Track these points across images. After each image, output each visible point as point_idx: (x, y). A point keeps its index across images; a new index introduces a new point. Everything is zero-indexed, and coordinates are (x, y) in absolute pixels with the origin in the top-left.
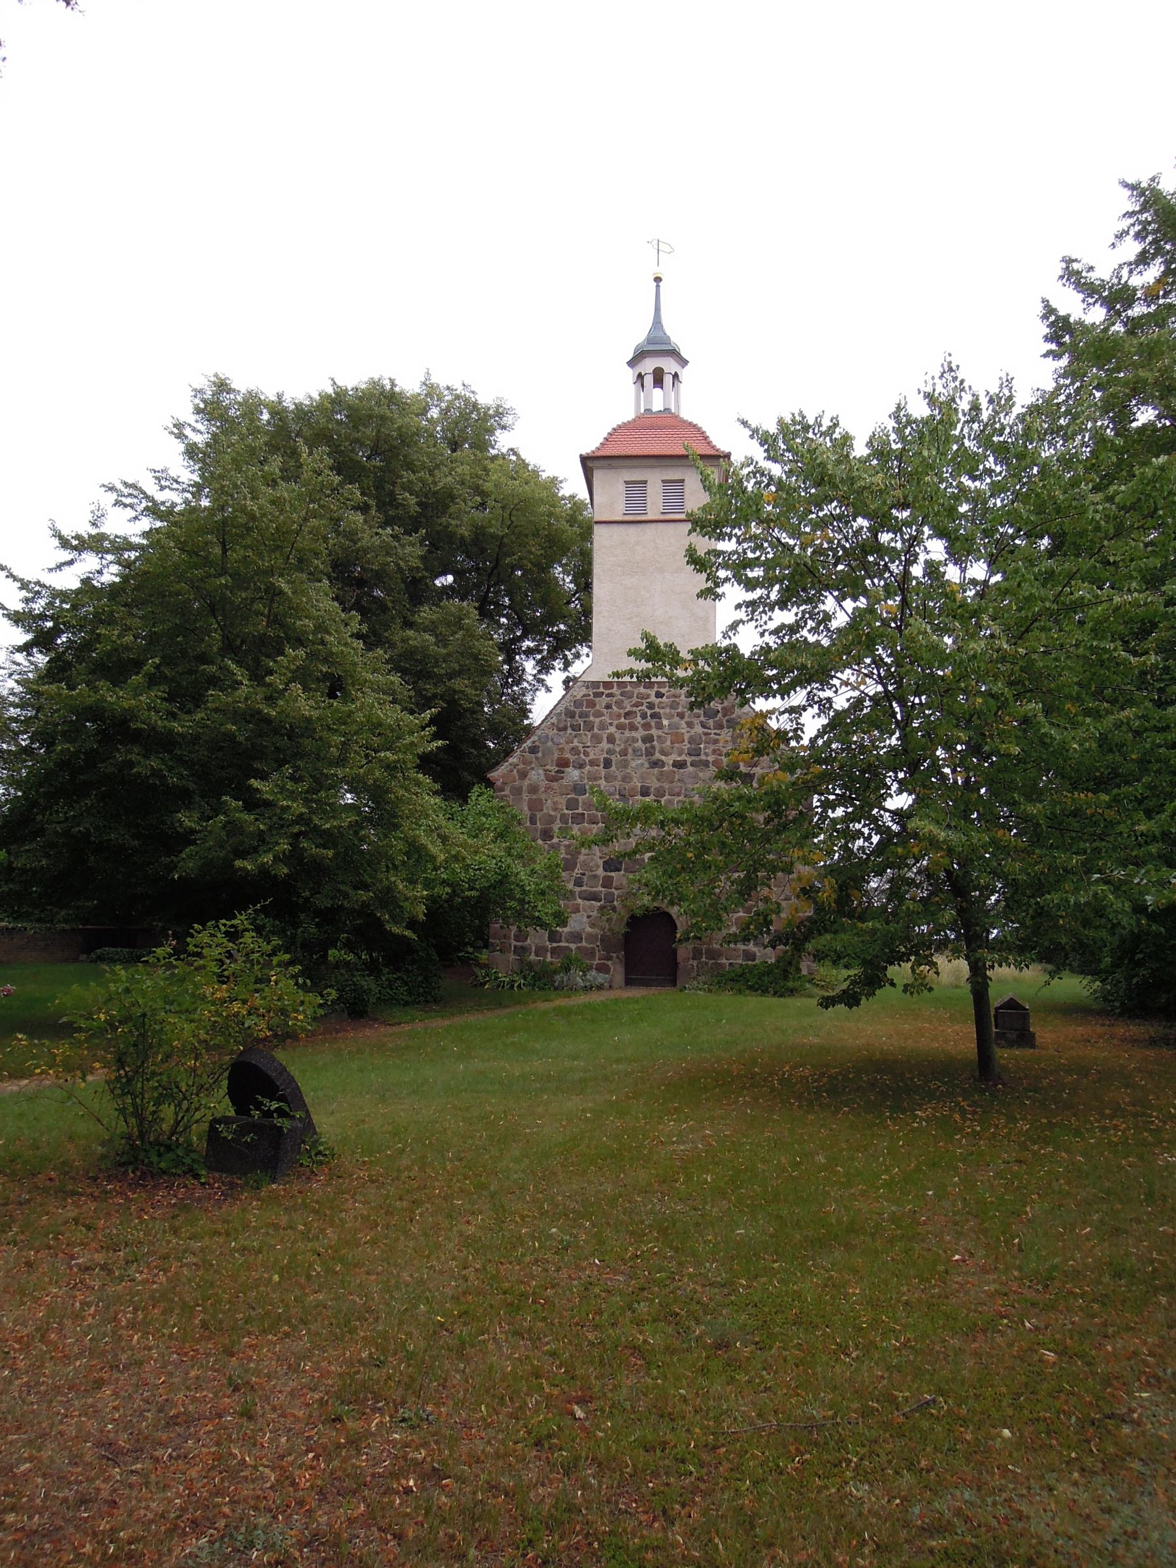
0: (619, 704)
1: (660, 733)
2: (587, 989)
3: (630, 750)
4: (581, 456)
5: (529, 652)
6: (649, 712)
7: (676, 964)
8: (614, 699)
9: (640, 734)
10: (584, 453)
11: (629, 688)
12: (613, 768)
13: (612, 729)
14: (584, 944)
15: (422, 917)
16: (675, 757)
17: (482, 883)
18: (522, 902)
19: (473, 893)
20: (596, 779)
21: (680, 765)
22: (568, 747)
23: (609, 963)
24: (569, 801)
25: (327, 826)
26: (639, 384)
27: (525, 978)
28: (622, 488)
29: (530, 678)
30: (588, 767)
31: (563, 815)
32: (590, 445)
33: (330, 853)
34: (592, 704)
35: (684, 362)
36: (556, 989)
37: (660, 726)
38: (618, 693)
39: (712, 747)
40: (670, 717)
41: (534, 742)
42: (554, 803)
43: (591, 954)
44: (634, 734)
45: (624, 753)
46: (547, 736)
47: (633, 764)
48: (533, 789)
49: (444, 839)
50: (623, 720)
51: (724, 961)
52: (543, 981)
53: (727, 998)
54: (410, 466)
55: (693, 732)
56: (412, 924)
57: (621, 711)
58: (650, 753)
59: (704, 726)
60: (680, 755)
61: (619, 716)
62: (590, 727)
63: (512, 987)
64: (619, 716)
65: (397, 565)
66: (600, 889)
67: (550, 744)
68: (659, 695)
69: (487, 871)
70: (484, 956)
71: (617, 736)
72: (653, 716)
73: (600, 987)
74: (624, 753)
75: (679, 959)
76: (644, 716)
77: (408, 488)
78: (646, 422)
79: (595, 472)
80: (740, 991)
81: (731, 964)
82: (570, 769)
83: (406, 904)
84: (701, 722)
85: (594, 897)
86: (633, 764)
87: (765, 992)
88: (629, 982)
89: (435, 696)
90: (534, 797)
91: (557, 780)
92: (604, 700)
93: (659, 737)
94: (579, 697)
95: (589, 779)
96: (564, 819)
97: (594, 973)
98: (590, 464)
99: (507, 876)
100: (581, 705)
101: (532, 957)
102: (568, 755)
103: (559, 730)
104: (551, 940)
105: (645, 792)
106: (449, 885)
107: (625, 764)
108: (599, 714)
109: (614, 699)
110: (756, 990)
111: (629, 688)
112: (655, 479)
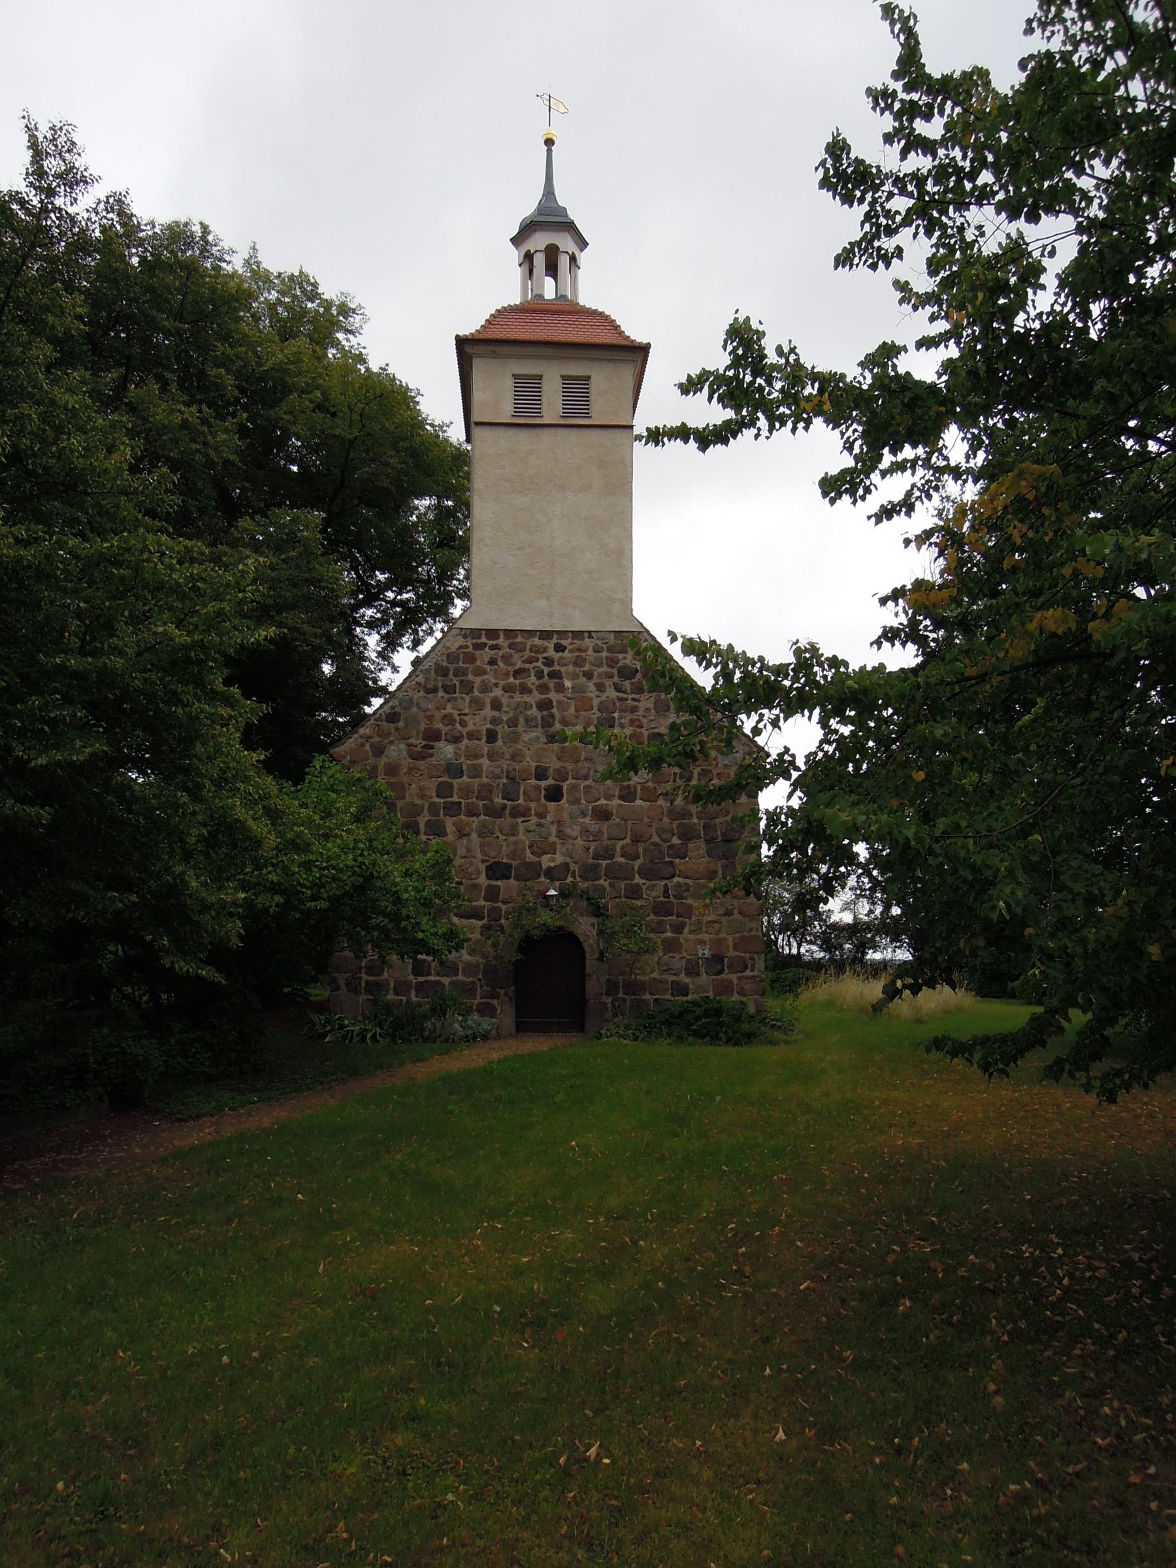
0: (507, 659)
1: (561, 697)
2: (470, 1039)
3: (521, 720)
4: (457, 336)
5: (372, 625)
6: (546, 670)
8: (501, 653)
9: (534, 698)
12: (499, 743)
13: (498, 692)
15: (235, 942)
17: (333, 889)
18: (396, 918)
19: (321, 905)
20: (476, 757)
22: (438, 715)
23: (495, 1002)
24: (440, 785)
25: (42, 761)
26: (526, 266)
28: (510, 382)
29: (373, 655)
30: (465, 742)
32: (471, 326)
33: (45, 814)
34: (471, 659)
35: (583, 244)
37: (560, 688)
38: (506, 644)
39: (629, 717)
40: (574, 677)
41: (393, 708)
42: (421, 788)
43: (470, 990)
45: (513, 723)
46: (411, 699)
48: (392, 770)
49: (274, 815)
50: (511, 680)
53: (664, 1049)
54: (225, 337)
55: (603, 697)
56: (219, 955)
58: (547, 723)
59: (618, 688)
61: (507, 674)
62: (468, 688)
63: (364, 1038)
65: (207, 455)
66: (482, 903)
67: (415, 709)
68: (559, 648)
69: (341, 871)
70: (317, 992)
72: (552, 675)
73: (485, 1037)
74: (513, 723)
76: (539, 675)
77: (224, 362)
78: (533, 308)
80: (680, 1039)
82: (442, 744)
83: (206, 919)
85: (476, 914)
86: (526, 737)
87: (715, 1039)
88: (523, 1027)
90: (394, 780)
91: (424, 758)
92: (487, 654)
93: (559, 702)
94: (453, 649)
95: (468, 757)
97: (476, 1016)
98: (468, 349)
99: (369, 878)
100: (457, 659)
101: (391, 996)
102: (440, 726)
103: (428, 691)
105: (541, 774)
106: (280, 892)
107: (514, 738)
108: (479, 672)
109: (501, 653)
110: (703, 1037)
112: (552, 378)
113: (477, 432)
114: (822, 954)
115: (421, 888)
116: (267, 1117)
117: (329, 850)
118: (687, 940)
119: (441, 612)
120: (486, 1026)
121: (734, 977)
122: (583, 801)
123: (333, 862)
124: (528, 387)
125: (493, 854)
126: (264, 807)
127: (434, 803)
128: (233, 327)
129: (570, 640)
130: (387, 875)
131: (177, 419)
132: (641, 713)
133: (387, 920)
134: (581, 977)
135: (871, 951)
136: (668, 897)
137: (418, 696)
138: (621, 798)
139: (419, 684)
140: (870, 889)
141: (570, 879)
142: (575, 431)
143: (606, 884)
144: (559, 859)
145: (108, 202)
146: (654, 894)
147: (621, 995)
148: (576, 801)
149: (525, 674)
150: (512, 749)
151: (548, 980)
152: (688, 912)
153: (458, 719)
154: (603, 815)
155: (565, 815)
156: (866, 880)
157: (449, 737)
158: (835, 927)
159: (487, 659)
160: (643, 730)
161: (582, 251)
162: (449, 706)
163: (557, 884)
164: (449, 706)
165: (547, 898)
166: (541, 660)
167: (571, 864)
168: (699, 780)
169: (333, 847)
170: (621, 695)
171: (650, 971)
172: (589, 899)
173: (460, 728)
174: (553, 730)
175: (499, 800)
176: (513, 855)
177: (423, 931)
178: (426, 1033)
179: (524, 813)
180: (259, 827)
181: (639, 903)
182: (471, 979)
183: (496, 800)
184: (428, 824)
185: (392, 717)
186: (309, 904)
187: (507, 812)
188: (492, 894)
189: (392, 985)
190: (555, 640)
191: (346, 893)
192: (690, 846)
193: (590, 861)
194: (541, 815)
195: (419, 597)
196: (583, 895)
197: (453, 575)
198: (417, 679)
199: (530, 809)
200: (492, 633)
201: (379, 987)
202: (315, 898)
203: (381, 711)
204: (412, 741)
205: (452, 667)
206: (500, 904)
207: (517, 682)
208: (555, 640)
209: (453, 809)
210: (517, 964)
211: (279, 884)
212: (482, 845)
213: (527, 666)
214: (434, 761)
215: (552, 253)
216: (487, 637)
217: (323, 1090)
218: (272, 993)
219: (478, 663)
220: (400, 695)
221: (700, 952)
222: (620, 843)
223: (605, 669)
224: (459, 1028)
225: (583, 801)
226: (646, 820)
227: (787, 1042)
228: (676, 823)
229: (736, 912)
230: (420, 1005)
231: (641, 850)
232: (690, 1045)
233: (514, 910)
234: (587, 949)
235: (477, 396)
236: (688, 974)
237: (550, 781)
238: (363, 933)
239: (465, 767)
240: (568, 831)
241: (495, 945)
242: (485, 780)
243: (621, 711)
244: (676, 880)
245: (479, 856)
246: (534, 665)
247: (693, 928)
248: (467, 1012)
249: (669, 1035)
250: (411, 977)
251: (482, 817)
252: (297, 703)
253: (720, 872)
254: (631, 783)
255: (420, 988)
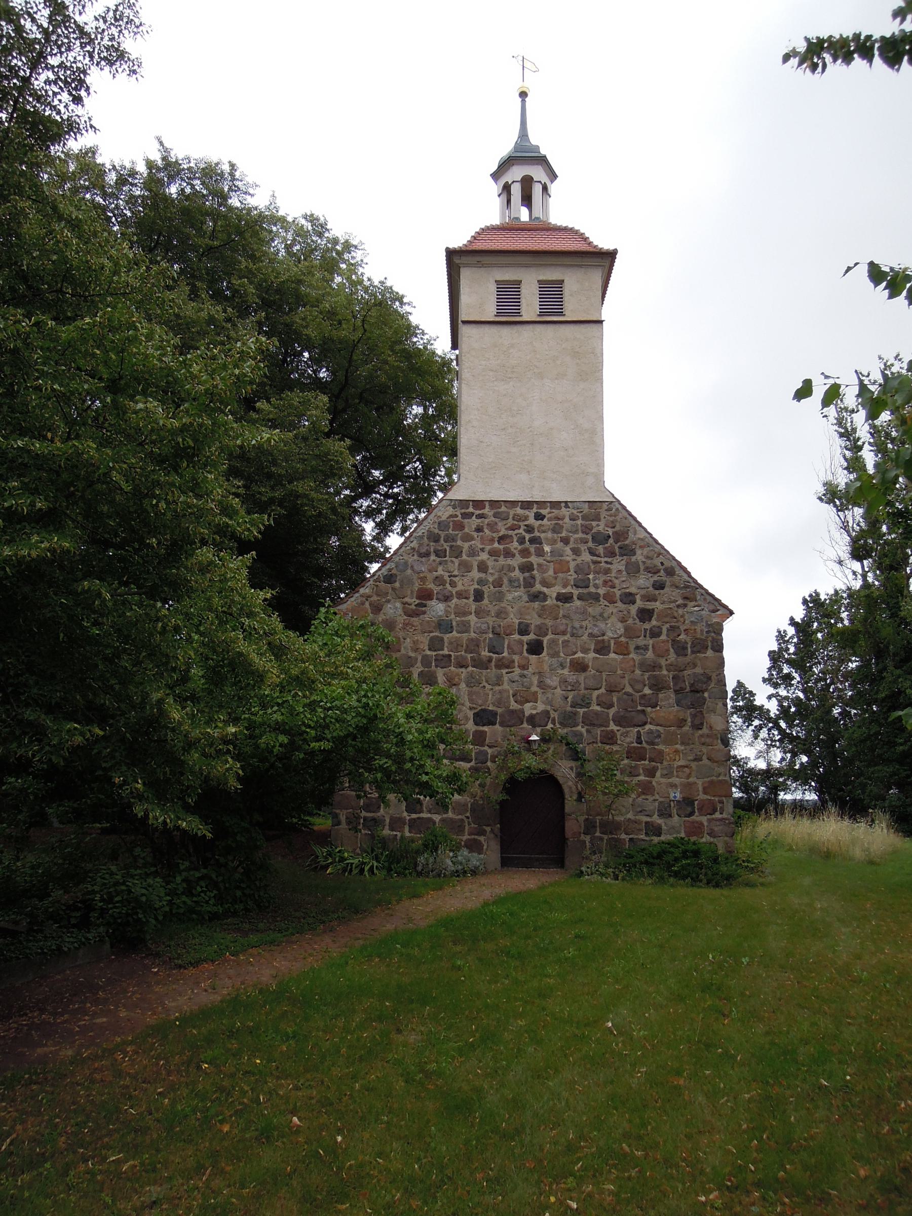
0: (492, 527)
1: (541, 560)
2: (461, 874)
3: (505, 581)
5: (369, 514)
6: (527, 537)
7: (563, 840)
8: (486, 521)
9: (517, 561)
10: (451, 247)
11: (503, 509)
12: (486, 601)
13: (484, 556)
14: (450, 814)
15: (234, 784)
16: (558, 589)
17: (337, 731)
18: (399, 760)
19: (325, 745)
21: (565, 598)
22: (430, 576)
23: (482, 838)
24: (432, 639)
26: (504, 196)
27: (377, 859)
28: (493, 288)
30: (455, 600)
31: (425, 657)
32: (459, 241)
34: (460, 526)
35: (553, 176)
36: (419, 874)
37: (540, 553)
38: (491, 514)
39: (603, 578)
40: (553, 542)
41: (390, 570)
42: (413, 643)
43: (458, 827)
44: (509, 561)
45: (498, 584)
46: (406, 563)
47: (509, 597)
50: (496, 545)
51: (623, 836)
52: (403, 863)
55: (579, 559)
57: (494, 535)
58: (529, 583)
59: (592, 553)
60: (565, 586)
61: (492, 540)
63: (362, 871)
64: (492, 540)
67: (409, 571)
69: (345, 711)
70: (321, 823)
71: (490, 563)
72: (533, 541)
73: (474, 872)
74: (498, 584)
75: (568, 833)
76: (522, 541)
78: (511, 228)
79: (461, 269)
81: (631, 839)
82: (433, 603)
84: (589, 549)
86: (509, 597)
87: (696, 880)
88: (506, 863)
89: (272, 501)
91: (418, 615)
92: (474, 522)
93: (540, 565)
94: (444, 518)
95: (457, 614)
96: (426, 661)
97: (465, 852)
98: (457, 260)
101: (386, 832)
102: (431, 586)
103: (421, 555)
104: (409, 810)
106: (284, 732)
107: (500, 597)
108: (467, 538)
109: (486, 521)
110: (684, 878)
111: (503, 509)
113: (464, 330)
114: (741, 795)
115: (424, 729)
116: (269, 967)
117: (334, 691)
118: (659, 783)
119: (424, 503)
120: (475, 862)
121: (704, 819)
122: (562, 654)
123: (337, 703)
124: (509, 294)
125: (480, 702)
126: (269, 644)
127: (427, 655)
128: (255, 247)
129: (548, 510)
130: (391, 716)
131: (204, 315)
132: (613, 575)
133: (390, 762)
134: (561, 816)
135: (782, 793)
136: (641, 743)
137: (412, 559)
138: (597, 651)
139: (413, 549)
140: (779, 740)
141: (550, 726)
142: (551, 328)
143: (584, 730)
144: (541, 707)
145: (115, 11)
146: (628, 740)
147: (598, 834)
148: (555, 655)
149: (508, 540)
150: (497, 607)
151: (531, 819)
152: (659, 757)
153: (448, 579)
154: (580, 667)
155: (546, 667)
156: (776, 733)
157: (440, 596)
158: (751, 772)
159: (474, 527)
160: (615, 590)
161: (552, 182)
162: (440, 568)
163: (539, 729)
164: (440, 568)
165: (530, 742)
166: (523, 527)
167: (552, 712)
168: (667, 635)
169: (337, 687)
170: (595, 558)
171: (625, 812)
172: (568, 744)
173: (450, 588)
174: (534, 590)
175: (485, 653)
176: (499, 703)
177: (427, 774)
178: (419, 868)
179: (509, 665)
180: (262, 661)
181: (615, 748)
182: (460, 817)
183: (483, 653)
184: (421, 674)
185: (389, 579)
186: (313, 745)
187: (493, 663)
188: (479, 739)
189: (388, 821)
190: (535, 510)
191: (349, 735)
192: (661, 696)
193: (569, 709)
194: (524, 667)
195: (407, 491)
196: (563, 740)
197: (436, 471)
198: (412, 545)
199: (513, 661)
200: (479, 504)
201: (376, 822)
202: (318, 739)
203: (379, 573)
204: (406, 600)
205: (442, 534)
206: (486, 748)
207: (501, 547)
208: (535, 510)
209: (444, 661)
210: (502, 803)
211: (284, 723)
212: (470, 694)
213: (510, 533)
214: (426, 617)
215: (527, 183)
216: (475, 507)
217: (325, 932)
218: (273, 831)
219: (466, 530)
220: (396, 559)
221: (672, 795)
222: (596, 693)
223: (580, 535)
224: (450, 863)
225: (562, 654)
226: (619, 672)
227: (762, 884)
228: (647, 675)
229: (704, 757)
230: (413, 841)
231: (615, 699)
232: (672, 886)
233: (499, 753)
234: (566, 791)
235: (465, 299)
236: (661, 815)
237: (532, 636)
238: (366, 774)
239: (454, 624)
240: (548, 681)
241: (482, 786)
242: (473, 635)
243: (596, 572)
244: (648, 727)
245: (468, 704)
246: (517, 531)
247: (665, 772)
248: (456, 848)
249: (650, 875)
250: (405, 814)
251: (470, 668)
252: (303, 566)
253: (689, 720)
254: (605, 638)
255: (413, 824)
